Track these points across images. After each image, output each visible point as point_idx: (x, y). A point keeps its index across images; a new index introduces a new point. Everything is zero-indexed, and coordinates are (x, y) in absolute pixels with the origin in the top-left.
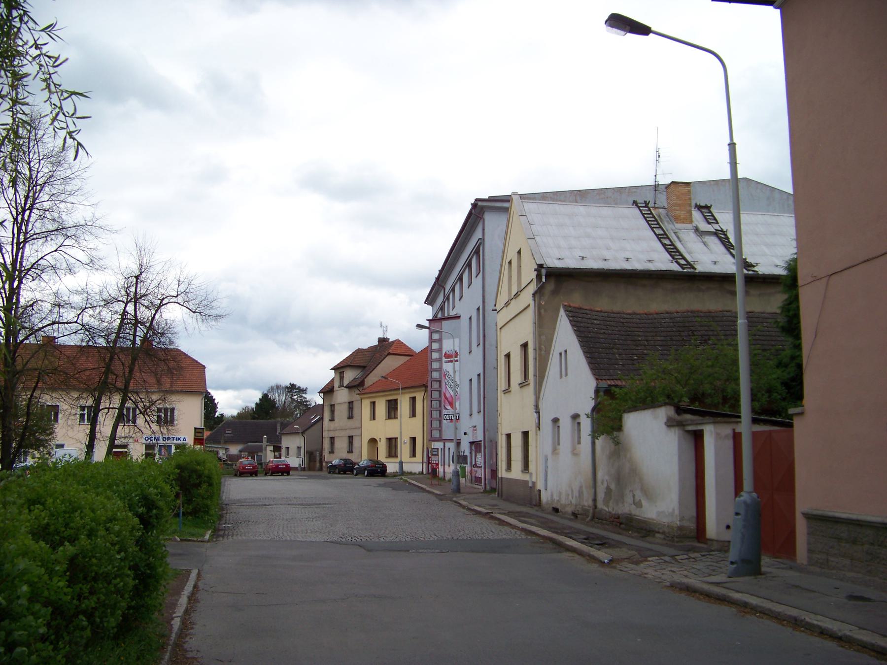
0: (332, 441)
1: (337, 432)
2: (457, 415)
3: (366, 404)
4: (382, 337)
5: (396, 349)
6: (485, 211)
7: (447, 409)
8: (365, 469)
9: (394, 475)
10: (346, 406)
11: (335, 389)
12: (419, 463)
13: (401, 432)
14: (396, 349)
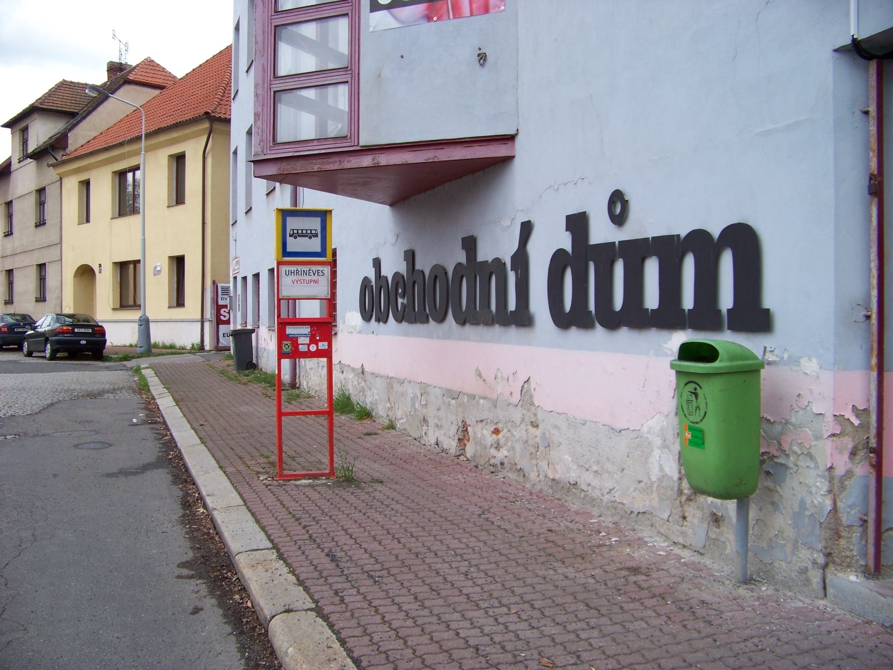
1: (17, 258)
3: (71, 185)
4: (116, 60)
5: (143, 74)
8: (47, 340)
9: (126, 355)
10: (32, 200)
11: (13, 167)
13: (144, 240)
14: (143, 74)
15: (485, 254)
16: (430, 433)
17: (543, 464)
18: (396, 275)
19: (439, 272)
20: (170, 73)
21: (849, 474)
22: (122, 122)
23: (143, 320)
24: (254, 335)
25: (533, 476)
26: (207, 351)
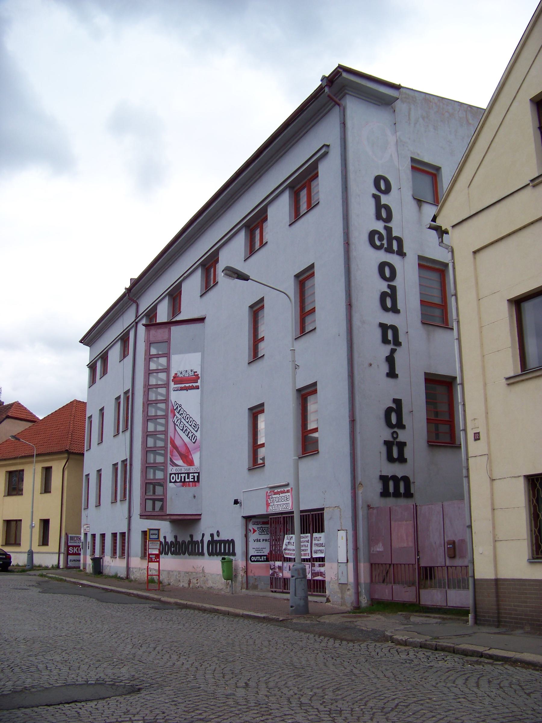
0: (443, 408)
2: (196, 475)
6: (346, 94)
7: (177, 465)
9: (23, 570)
12: (53, 553)
15: (195, 539)
16: (181, 584)
17: (206, 584)
18: (171, 542)
19: (184, 542)
20: (29, 411)
21: (244, 575)
22: (8, 443)
23: (31, 552)
24: (101, 560)
25: (204, 587)
26: (61, 569)
